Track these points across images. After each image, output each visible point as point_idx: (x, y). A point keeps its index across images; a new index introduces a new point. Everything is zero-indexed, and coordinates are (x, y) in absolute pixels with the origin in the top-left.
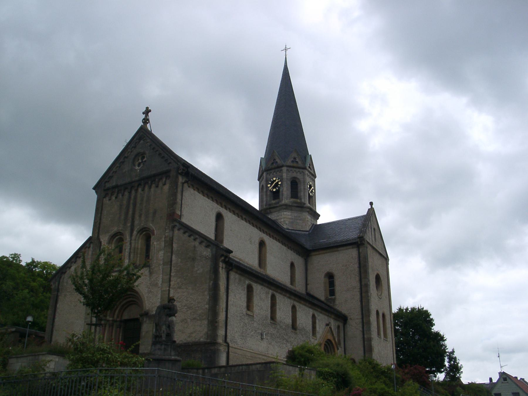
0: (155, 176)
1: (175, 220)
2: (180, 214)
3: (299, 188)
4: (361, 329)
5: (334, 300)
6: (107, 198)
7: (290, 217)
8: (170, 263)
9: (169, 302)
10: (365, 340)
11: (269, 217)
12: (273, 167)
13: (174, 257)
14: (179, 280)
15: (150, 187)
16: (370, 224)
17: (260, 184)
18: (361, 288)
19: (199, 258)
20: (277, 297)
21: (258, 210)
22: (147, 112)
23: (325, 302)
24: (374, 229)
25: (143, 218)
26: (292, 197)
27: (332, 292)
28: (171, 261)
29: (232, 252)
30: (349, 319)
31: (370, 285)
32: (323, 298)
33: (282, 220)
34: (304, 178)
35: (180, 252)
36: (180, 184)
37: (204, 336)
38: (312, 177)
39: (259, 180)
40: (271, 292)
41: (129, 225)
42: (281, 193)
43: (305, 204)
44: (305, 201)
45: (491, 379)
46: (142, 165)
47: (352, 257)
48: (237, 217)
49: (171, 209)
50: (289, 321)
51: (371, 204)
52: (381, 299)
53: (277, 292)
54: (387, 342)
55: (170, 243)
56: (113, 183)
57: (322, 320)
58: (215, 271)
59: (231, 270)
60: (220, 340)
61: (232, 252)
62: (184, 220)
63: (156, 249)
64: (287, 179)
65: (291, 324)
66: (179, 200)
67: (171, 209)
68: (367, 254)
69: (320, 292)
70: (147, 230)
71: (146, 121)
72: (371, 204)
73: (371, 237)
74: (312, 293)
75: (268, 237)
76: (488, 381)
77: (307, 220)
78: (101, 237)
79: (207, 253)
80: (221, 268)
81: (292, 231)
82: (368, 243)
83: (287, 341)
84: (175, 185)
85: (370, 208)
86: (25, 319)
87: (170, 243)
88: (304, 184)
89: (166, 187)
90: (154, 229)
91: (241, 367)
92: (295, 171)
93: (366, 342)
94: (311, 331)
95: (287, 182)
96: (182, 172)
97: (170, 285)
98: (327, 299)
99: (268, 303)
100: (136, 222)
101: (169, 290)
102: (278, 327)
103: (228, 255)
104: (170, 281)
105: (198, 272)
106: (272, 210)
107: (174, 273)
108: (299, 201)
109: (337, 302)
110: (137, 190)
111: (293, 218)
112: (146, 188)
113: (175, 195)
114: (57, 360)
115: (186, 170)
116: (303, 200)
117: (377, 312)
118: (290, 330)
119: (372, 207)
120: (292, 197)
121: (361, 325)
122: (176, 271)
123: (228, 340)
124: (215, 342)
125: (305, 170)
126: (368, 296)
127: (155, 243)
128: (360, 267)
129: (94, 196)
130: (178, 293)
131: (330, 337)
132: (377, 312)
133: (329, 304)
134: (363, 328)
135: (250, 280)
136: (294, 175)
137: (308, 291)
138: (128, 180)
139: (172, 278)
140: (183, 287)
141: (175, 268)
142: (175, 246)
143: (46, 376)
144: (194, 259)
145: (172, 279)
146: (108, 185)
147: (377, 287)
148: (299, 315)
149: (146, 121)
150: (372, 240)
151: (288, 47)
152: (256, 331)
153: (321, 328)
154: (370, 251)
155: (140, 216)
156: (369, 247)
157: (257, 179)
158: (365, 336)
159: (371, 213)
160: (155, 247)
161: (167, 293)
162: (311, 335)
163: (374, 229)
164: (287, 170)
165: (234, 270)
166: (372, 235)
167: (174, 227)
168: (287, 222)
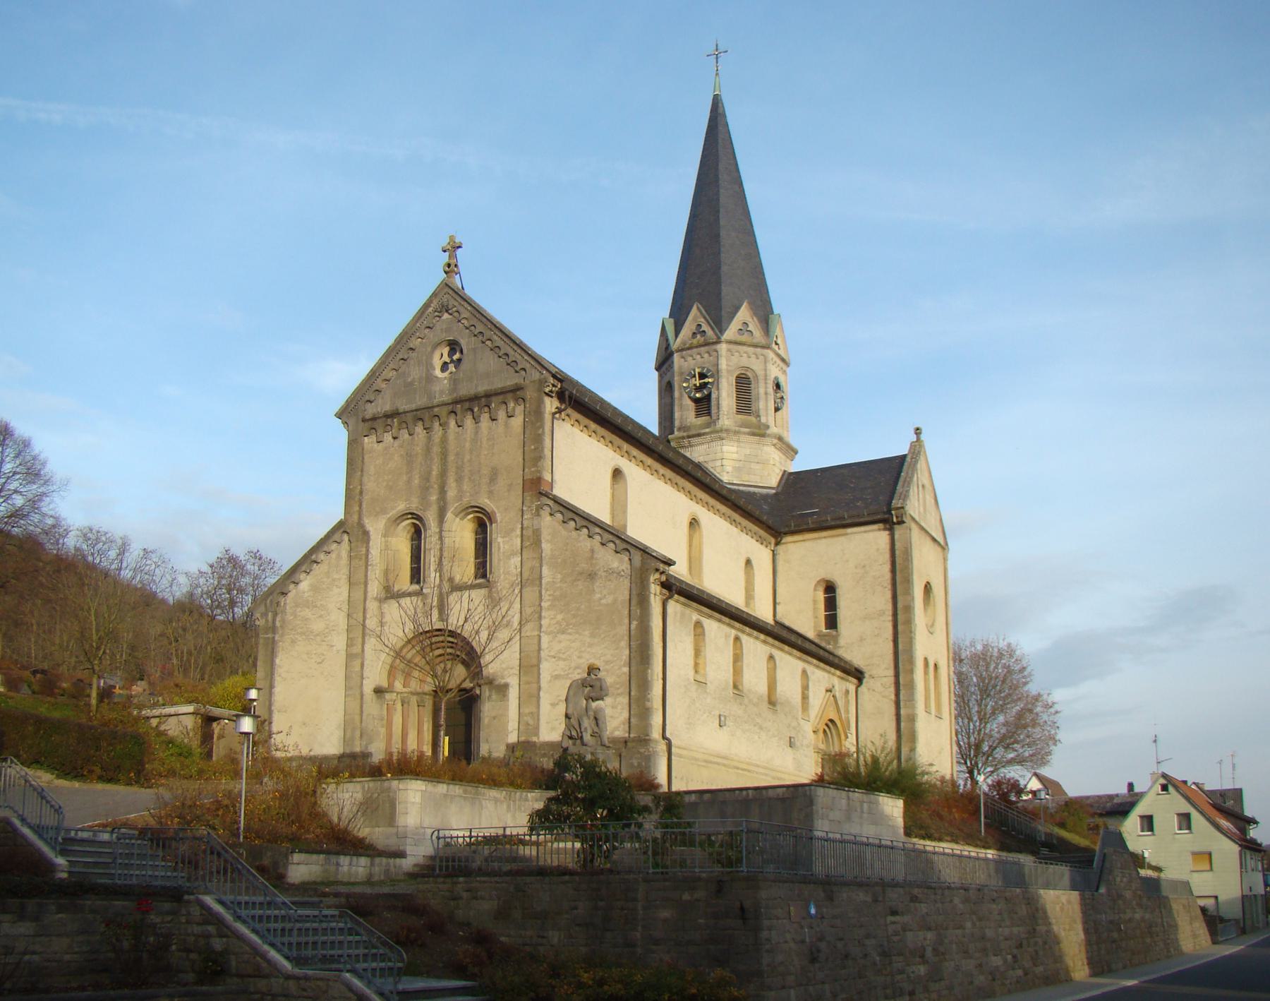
0: (488, 395)
1: (546, 495)
2: (550, 481)
3: (753, 393)
4: (893, 697)
5: (835, 639)
6: (373, 438)
7: (735, 456)
8: (538, 583)
9: (589, 674)
10: (902, 719)
11: (688, 454)
12: (695, 341)
13: (545, 570)
14: (560, 617)
15: (476, 420)
16: (915, 479)
17: (661, 377)
18: (895, 615)
19: (604, 574)
20: (743, 641)
21: (657, 434)
22: (453, 248)
23: (817, 641)
24: (923, 486)
25: (466, 486)
26: (739, 412)
27: (832, 622)
28: (541, 578)
29: (674, 563)
30: (866, 675)
31: (914, 608)
32: (810, 634)
33: (718, 463)
34: (766, 370)
35: (559, 560)
36: (548, 417)
37: (622, 726)
38: (782, 364)
39: (658, 369)
40: (733, 632)
41: (434, 498)
42: (713, 403)
43: (768, 427)
44: (767, 420)
45: (1131, 786)
46: (452, 368)
47: (878, 550)
48: (649, 475)
49: (533, 469)
50: (763, 688)
51: (918, 431)
52: (932, 633)
53: (743, 632)
54: (942, 721)
55: (532, 541)
56: (383, 405)
57: (821, 678)
58: (640, 599)
59: (670, 597)
60: (656, 734)
61: (674, 563)
62: (558, 491)
63: (501, 550)
64: (728, 371)
65: (766, 693)
66: (547, 452)
67: (533, 469)
68: (911, 543)
69: (807, 622)
70: (490, 519)
71: (451, 269)
72: (918, 431)
73: (916, 505)
74: (787, 623)
75: (704, 510)
76: (1123, 790)
77: (772, 462)
78: (367, 521)
79: (620, 563)
80: (652, 596)
81: (741, 488)
82: (913, 519)
83: (761, 728)
84: (535, 415)
85: (915, 440)
86: (245, 694)
87: (532, 541)
88: (766, 383)
89: (517, 421)
90: (496, 511)
91: (744, 793)
92: (745, 353)
93: (903, 724)
94: (800, 704)
95: (728, 378)
96: (551, 391)
97: (541, 626)
98: (820, 635)
99: (763, 665)
100: (451, 493)
101: (540, 636)
102: (746, 701)
103: (667, 568)
104: (540, 618)
105: (603, 601)
106: (694, 440)
107: (549, 603)
108: (753, 419)
109: (842, 642)
110: (444, 425)
111: (742, 458)
112: (469, 421)
113: (538, 439)
114: (424, 788)
115: (559, 386)
116: (763, 420)
117: (926, 660)
118: (765, 705)
119: (918, 439)
120: (739, 412)
121: (892, 689)
122: (551, 598)
123: (668, 735)
124: (647, 738)
125: (769, 351)
126: (911, 632)
127: (500, 540)
128: (893, 571)
129: (339, 435)
130: (560, 642)
131: (833, 716)
132: (926, 660)
133: (823, 644)
134: (897, 694)
135: (700, 612)
136: (745, 361)
137: (778, 618)
138: (420, 401)
139: (543, 611)
140: (570, 631)
141: (548, 593)
142: (546, 547)
143: (688, 841)
144: (592, 576)
145: (543, 614)
146: (371, 410)
147: (925, 609)
148: (781, 675)
149: (451, 269)
150: (919, 512)
151: (721, 48)
152: (710, 713)
153: (817, 698)
154: (916, 534)
155: (459, 480)
156: (913, 526)
157: (654, 367)
158: (903, 712)
159: (917, 447)
160: (499, 548)
161: (536, 641)
162: (800, 713)
163: (923, 486)
164: (729, 350)
165: (676, 596)
166: (919, 501)
167: (539, 508)
168: (729, 469)
